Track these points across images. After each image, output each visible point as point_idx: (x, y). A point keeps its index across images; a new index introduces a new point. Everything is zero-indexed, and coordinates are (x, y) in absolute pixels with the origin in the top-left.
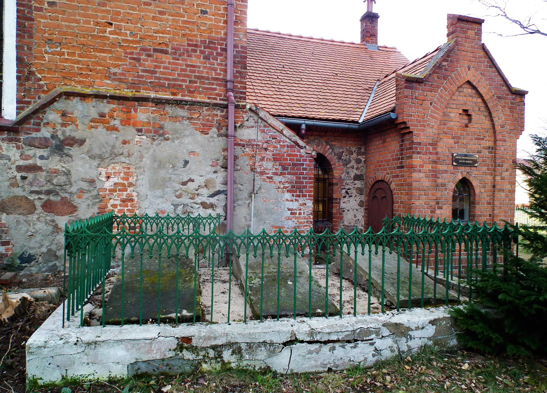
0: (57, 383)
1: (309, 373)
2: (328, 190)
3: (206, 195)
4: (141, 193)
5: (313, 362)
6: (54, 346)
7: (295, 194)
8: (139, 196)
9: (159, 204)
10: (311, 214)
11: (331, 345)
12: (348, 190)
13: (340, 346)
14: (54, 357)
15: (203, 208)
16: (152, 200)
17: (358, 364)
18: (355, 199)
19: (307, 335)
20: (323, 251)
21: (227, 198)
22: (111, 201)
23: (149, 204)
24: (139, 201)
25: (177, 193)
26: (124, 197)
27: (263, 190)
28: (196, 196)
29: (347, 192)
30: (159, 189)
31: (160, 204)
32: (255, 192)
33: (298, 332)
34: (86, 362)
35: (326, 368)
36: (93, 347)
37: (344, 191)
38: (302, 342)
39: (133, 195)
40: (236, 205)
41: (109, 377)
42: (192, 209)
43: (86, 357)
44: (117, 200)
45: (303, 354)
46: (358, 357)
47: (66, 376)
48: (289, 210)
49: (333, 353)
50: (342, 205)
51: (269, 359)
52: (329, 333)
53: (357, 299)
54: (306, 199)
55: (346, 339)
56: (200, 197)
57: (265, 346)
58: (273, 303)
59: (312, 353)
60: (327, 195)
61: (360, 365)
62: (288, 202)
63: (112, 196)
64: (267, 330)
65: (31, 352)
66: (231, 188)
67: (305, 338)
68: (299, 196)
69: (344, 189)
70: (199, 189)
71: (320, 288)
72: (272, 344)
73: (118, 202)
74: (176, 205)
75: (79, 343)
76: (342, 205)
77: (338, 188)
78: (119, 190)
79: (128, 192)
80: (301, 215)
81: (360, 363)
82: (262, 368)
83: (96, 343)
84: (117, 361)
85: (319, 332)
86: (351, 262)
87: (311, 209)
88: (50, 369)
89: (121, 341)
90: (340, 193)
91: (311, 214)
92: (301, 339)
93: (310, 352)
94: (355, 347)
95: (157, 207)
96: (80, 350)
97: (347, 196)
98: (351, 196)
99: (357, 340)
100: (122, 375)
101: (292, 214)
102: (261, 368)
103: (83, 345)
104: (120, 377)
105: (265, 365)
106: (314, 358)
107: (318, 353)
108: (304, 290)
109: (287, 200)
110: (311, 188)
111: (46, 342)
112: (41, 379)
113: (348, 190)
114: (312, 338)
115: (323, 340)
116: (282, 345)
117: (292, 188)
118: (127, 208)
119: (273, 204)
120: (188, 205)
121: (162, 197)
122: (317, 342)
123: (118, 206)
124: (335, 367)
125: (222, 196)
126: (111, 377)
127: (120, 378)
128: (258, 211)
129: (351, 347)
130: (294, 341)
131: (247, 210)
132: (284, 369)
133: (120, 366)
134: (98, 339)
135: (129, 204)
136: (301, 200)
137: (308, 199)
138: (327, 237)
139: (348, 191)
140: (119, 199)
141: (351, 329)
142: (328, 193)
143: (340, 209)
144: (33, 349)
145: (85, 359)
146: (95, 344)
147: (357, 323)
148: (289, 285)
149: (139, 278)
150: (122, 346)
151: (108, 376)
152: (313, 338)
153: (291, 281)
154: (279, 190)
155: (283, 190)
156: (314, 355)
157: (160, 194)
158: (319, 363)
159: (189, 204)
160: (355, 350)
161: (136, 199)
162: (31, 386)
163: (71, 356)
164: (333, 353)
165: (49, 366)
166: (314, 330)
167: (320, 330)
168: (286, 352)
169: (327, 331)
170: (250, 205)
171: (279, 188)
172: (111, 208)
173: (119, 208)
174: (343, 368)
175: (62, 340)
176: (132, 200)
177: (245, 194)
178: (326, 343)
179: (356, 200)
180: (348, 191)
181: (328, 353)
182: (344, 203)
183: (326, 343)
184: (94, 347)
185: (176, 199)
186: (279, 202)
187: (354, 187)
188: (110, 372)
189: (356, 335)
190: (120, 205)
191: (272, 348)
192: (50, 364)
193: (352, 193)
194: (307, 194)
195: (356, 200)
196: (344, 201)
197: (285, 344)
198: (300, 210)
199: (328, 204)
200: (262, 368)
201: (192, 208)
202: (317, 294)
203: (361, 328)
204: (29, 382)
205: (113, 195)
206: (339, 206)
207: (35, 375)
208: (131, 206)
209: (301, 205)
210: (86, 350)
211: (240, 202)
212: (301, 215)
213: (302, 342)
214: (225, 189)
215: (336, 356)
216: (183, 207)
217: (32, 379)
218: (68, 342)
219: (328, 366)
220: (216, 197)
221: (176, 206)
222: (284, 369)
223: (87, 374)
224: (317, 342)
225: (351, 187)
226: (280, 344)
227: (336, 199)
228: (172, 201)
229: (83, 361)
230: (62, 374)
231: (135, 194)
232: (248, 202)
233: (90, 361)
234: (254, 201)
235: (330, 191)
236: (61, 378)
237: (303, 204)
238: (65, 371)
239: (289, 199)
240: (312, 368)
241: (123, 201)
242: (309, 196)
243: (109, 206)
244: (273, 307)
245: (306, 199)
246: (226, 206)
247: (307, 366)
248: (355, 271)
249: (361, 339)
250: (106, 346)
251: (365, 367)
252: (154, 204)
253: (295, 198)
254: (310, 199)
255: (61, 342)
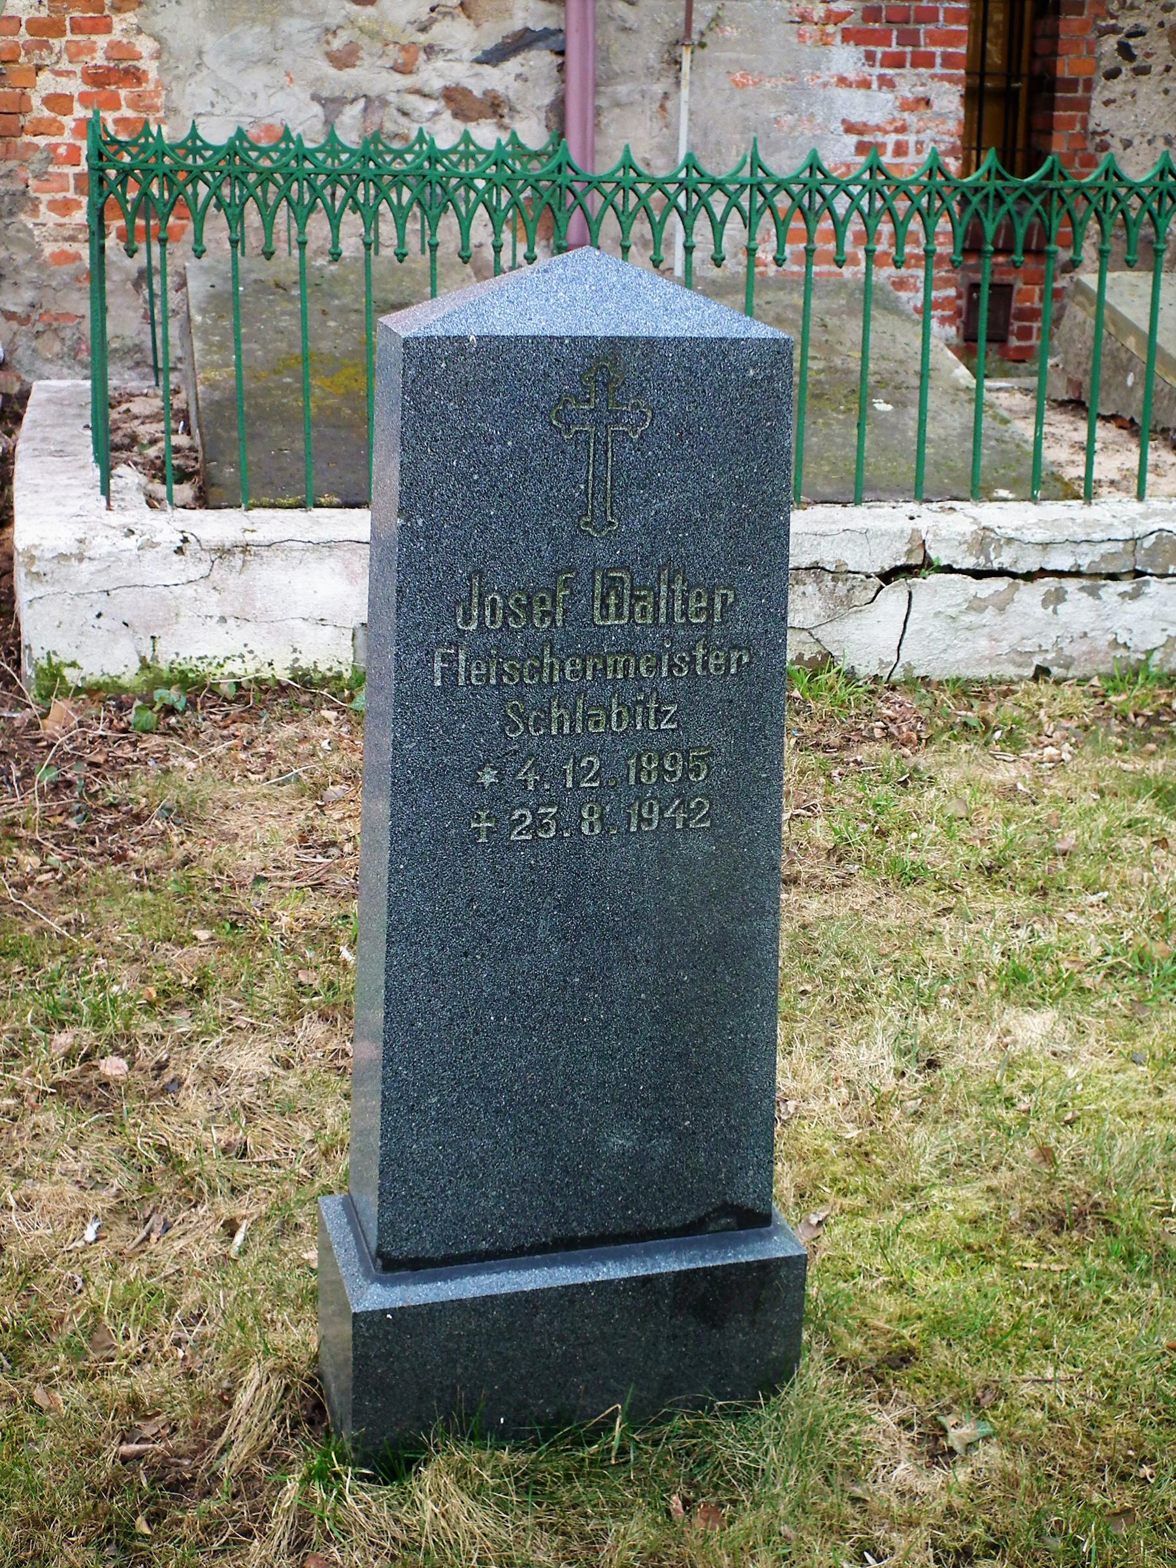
0: (125, 681)
1: (969, 681)
2: (1034, 37)
3: (467, 55)
4: (174, 43)
5: (983, 644)
6: (110, 554)
7: (879, 51)
8: (165, 57)
9: (255, 95)
10: (952, 152)
11: (1051, 582)
12: (1130, 35)
13: (1082, 589)
14: (113, 593)
15: (455, 115)
16: (226, 74)
17: (1143, 657)
18: (1166, 84)
19: (964, 547)
20: (995, 346)
21: (561, 68)
22: (44, 77)
23: (212, 96)
24: (167, 79)
25: (337, 44)
26: (99, 59)
27: (730, 32)
28: (422, 56)
29: (1125, 51)
30: (254, 20)
31: (262, 96)
32: (695, 37)
33: (935, 535)
34: (217, 613)
35: (1029, 665)
36: (237, 561)
37: (1110, 43)
38: (949, 569)
39: (138, 48)
40: (603, 102)
41: (293, 669)
42: (403, 120)
43: (215, 596)
44: (68, 73)
45: (952, 611)
46: (1144, 633)
47: (154, 658)
48: (850, 128)
49: (1055, 612)
50: (1100, 116)
51: (829, 627)
52: (1045, 545)
53: (1150, 477)
54: (933, 77)
55: (1105, 569)
56: (439, 63)
57: (818, 581)
58: (827, 468)
59: (981, 610)
60: (1024, 69)
61: (1151, 662)
62: (843, 93)
63: (45, 53)
64: (824, 528)
65: (37, 574)
66: (584, 19)
67: (959, 559)
68: (896, 61)
69: (1114, 30)
70: (432, 21)
71: (1003, 427)
72: (840, 573)
73: (74, 86)
74: (333, 100)
75: (189, 548)
76: (1100, 116)
77: (1084, 28)
78: (77, 27)
79: (116, 35)
80: (905, 154)
81: (1149, 652)
82: (806, 658)
83: (245, 548)
84: (317, 614)
85: (1010, 540)
86: (1131, 342)
87: (952, 125)
88: (100, 632)
89: (330, 545)
90: (1091, 51)
91: (952, 152)
92: (944, 562)
93: (976, 605)
94: (1135, 595)
95: (250, 111)
96: (195, 572)
97: (1126, 68)
98: (1143, 71)
99: (1143, 574)
100: (335, 664)
101: (861, 148)
102: (800, 657)
103: (205, 556)
104: (330, 669)
105: (816, 648)
106: (987, 630)
107: (1002, 610)
108: (941, 432)
109: (842, 81)
110: (957, 21)
111: (81, 541)
112: (73, 664)
113: (1130, 35)
114: (982, 560)
115: (1022, 568)
116: (878, 581)
117: (865, 19)
118: (117, 114)
119: (777, 100)
120: (385, 103)
121: (270, 62)
122: (1001, 573)
123: (76, 106)
124: (1060, 666)
125: (540, 60)
126: (301, 668)
127: (329, 674)
128: (705, 135)
129: (1123, 595)
130: (920, 567)
131: (657, 124)
132: (881, 662)
133: (329, 629)
134: (249, 537)
135: (123, 93)
136: (909, 83)
137: (942, 78)
138: (1052, 191)
139: (1132, 42)
140: (78, 68)
141: (1124, 533)
142: (1033, 55)
143: (1086, 134)
144: (42, 564)
145: (212, 604)
146: (243, 552)
147: (1145, 516)
148: (883, 413)
149: (288, 380)
150: (331, 562)
151: (288, 665)
152: (988, 559)
153: (887, 402)
154: (808, 28)
155: (824, 34)
156: (989, 615)
157: (257, 48)
158: (1004, 647)
159: (392, 97)
160: (1137, 606)
161: (150, 66)
162: (45, 688)
163: (166, 591)
164: (1055, 612)
165: (97, 622)
166: (992, 530)
167: (1012, 534)
168: (894, 597)
169: (1040, 537)
170: (669, 104)
171: (804, 19)
172: (46, 113)
173: (79, 112)
174: (1087, 669)
175: (133, 538)
176: (134, 76)
177: (650, 52)
178: (1029, 577)
179: (1166, 92)
180: (1132, 42)
181: (1039, 611)
182: (1107, 103)
183: (1029, 577)
184: (240, 563)
185: (332, 71)
186: (804, 90)
187: (1161, 25)
188: (295, 650)
189: (1140, 554)
190: (84, 99)
191: (842, 588)
192: (99, 615)
193: (1148, 55)
194: (938, 50)
195: (1166, 92)
196: (1107, 95)
197: (887, 577)
198: (902, 129)
199: (1030, 111)
200: (806, 658)
201: (405, 114)
202: (993, 443)
203: (1161, 530)
204: (37, 676)
205: (50, 49)
206: (1085, 122)
207: (55, 653)
208: (134, 104)
209: (906, 106)
210: (214, 572)
211: (622, 90)
212: (905, 154)
213: (949, 569)
214: (551, 24)
215: (1066, 626)
216: (365, 109)
217: (44, 663)
218: (154, 545)
219: (1037, 660)
220: (513, 65)
221: (332, 104)
222: (881, 662)
223: (222, 655)
224: (1001, 573)
225: (1145, 23)
226: (868, 577)
227: (1072, 85)
228: (311, 84)
229: (205, 611)
230: (138, 653)
231: (145, 45)
232: (658, 89)
233: (228, 610)
234: (691, 83)
235: (1042, 46)
236: (139, 665)
237: (918, 101)
238: (150, 642)
239: (852, 76)
240: (979, 662)
241: (97, 78)
242: (948, 60)
243: (36, 101)
244: (826, 477)
245: (933, 77)
246: (559, 108)
247: (961, 655)
248: (1148, 376)
249: (1159, 571)
250: (278, 562)
251: (1166, 670)
252: (233, 97)
253: (878, 70)
254: (950, 79)
255: (132, 543)
